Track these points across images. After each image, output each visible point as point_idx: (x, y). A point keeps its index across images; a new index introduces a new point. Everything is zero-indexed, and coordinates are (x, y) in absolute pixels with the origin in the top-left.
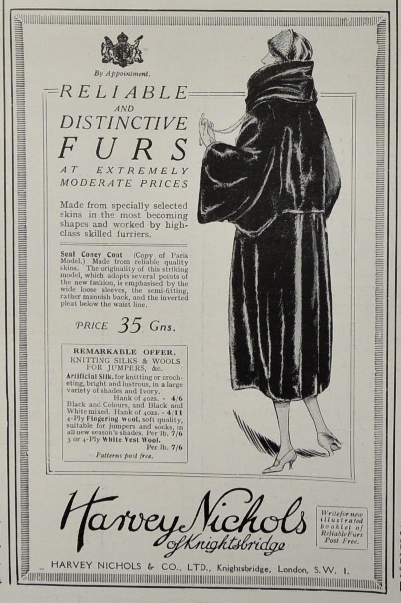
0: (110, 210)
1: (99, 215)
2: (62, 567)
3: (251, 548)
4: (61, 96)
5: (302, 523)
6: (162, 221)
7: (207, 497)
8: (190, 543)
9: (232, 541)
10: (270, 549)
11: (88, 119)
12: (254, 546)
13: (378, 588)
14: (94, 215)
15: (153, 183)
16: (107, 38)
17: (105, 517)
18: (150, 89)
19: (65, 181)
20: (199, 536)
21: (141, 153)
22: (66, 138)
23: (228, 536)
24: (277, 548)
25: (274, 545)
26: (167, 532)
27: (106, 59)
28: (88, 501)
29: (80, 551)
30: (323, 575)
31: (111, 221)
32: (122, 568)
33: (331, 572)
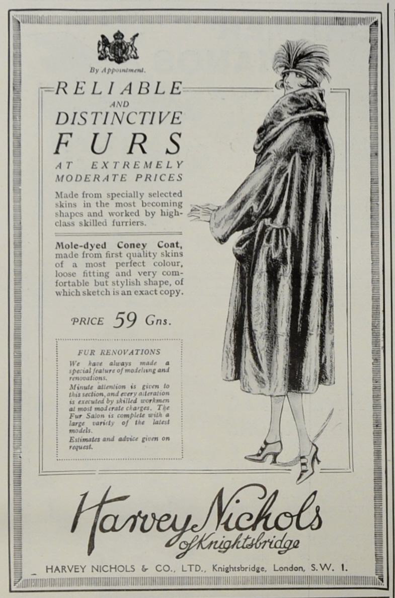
0: (105, 199)
1: (93, 205)
2: (57, 572)
3: (265, 547)
4: (57, 93)
5: (317, 519)
6: (158, 210)
7: (220, 496)
8: (203, 543)
9: (246, 540)
10: (285, 547)
11: (84, 115)
12: (268, 544)
13: (379, 584)
14: (88, 205)
15: (148, 177)
16: (103, 36)
17: (116, 518)
18: (145, 85)
19: (60, 177)
20: (212, 535)
21: (137, 148)
22: (61, 135)
23: (241, 534)
24: (292, 546)
25: (289, 542)
26: (179, 532)
27: (102, 56)
28: (99, 502)
29: (91, 555)
30: (320, 573)
31: (106, 211)
32: (116, 571)
33: (328, 569)
